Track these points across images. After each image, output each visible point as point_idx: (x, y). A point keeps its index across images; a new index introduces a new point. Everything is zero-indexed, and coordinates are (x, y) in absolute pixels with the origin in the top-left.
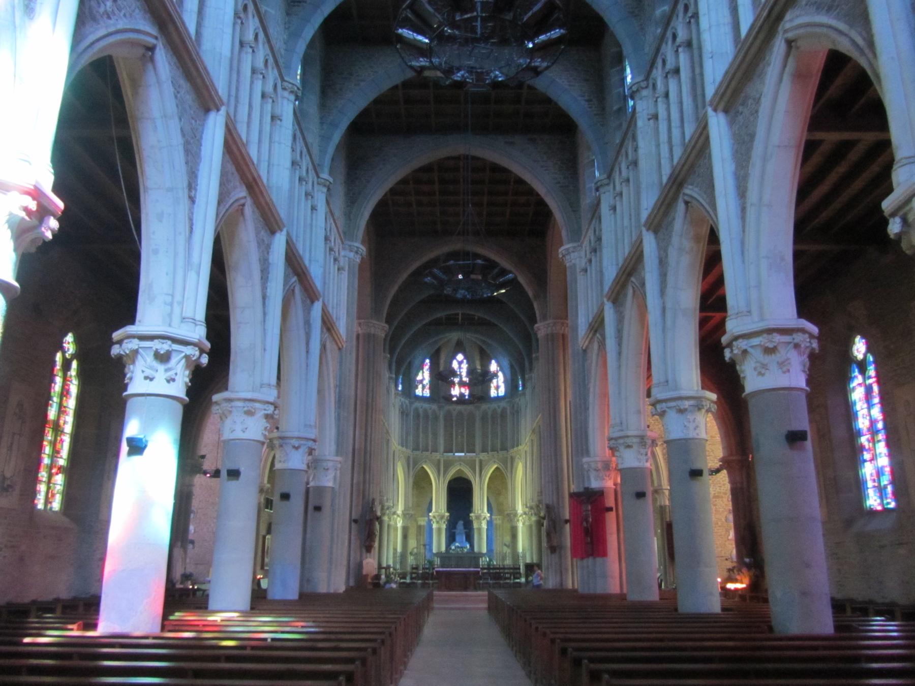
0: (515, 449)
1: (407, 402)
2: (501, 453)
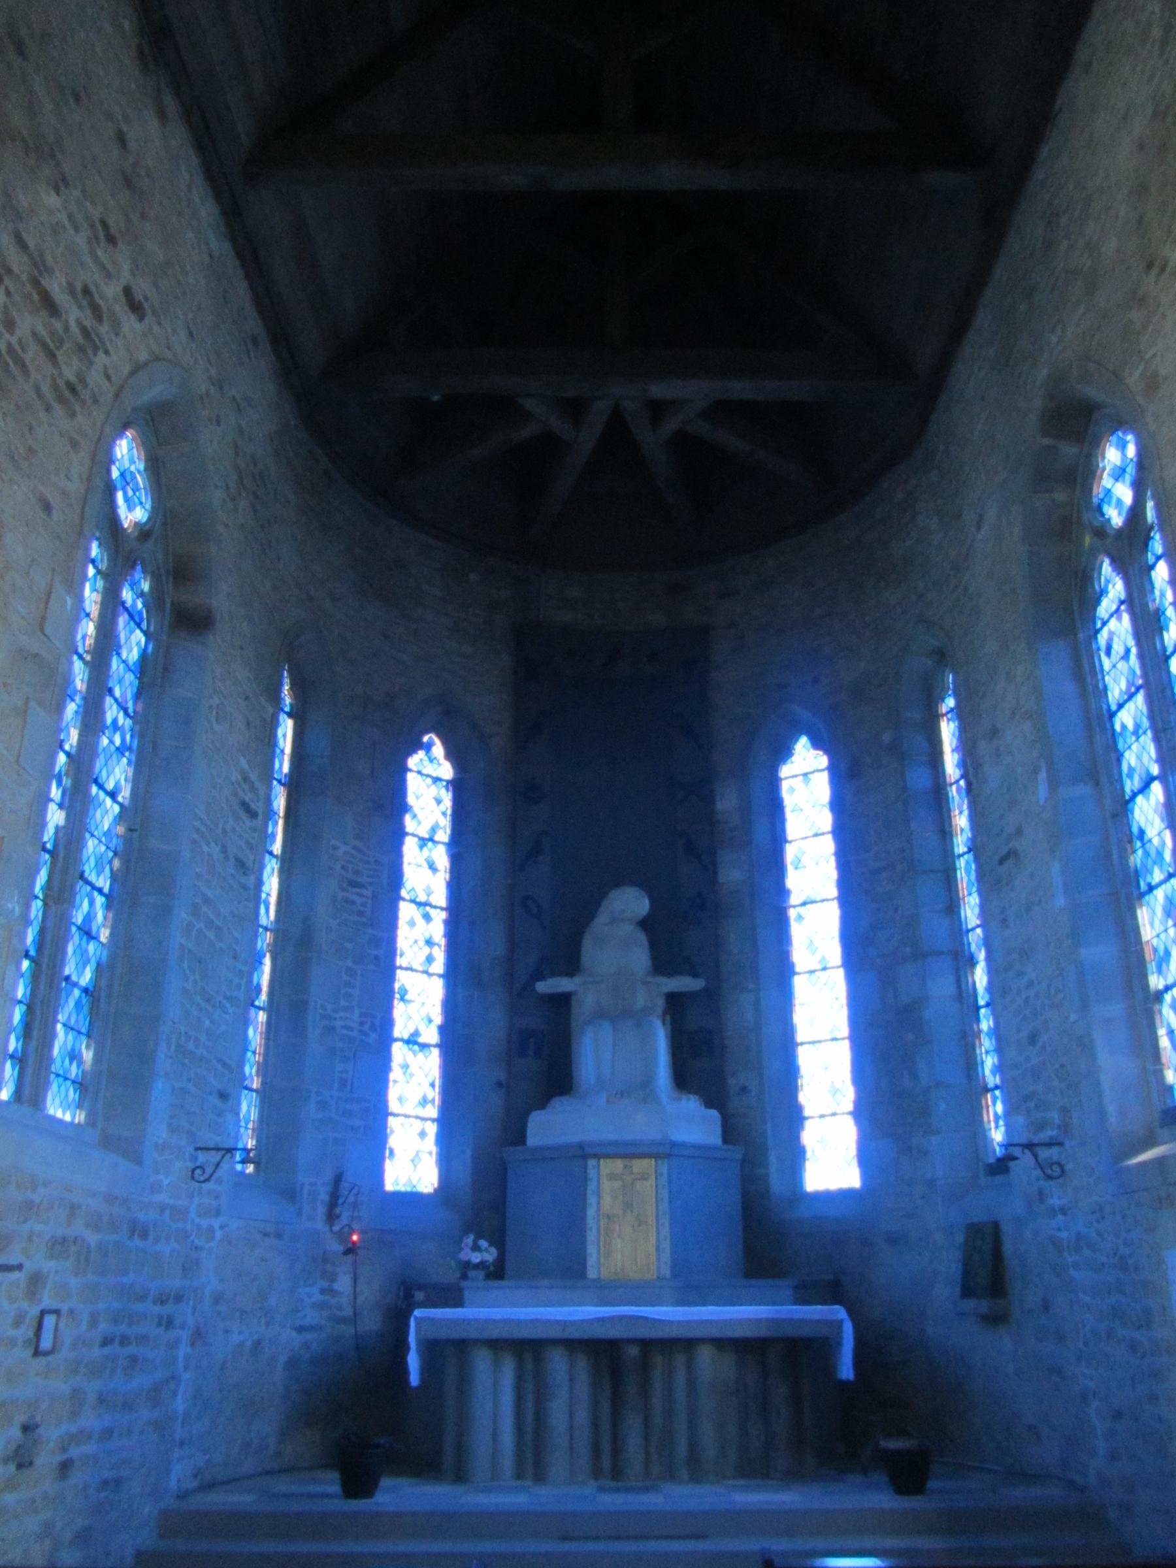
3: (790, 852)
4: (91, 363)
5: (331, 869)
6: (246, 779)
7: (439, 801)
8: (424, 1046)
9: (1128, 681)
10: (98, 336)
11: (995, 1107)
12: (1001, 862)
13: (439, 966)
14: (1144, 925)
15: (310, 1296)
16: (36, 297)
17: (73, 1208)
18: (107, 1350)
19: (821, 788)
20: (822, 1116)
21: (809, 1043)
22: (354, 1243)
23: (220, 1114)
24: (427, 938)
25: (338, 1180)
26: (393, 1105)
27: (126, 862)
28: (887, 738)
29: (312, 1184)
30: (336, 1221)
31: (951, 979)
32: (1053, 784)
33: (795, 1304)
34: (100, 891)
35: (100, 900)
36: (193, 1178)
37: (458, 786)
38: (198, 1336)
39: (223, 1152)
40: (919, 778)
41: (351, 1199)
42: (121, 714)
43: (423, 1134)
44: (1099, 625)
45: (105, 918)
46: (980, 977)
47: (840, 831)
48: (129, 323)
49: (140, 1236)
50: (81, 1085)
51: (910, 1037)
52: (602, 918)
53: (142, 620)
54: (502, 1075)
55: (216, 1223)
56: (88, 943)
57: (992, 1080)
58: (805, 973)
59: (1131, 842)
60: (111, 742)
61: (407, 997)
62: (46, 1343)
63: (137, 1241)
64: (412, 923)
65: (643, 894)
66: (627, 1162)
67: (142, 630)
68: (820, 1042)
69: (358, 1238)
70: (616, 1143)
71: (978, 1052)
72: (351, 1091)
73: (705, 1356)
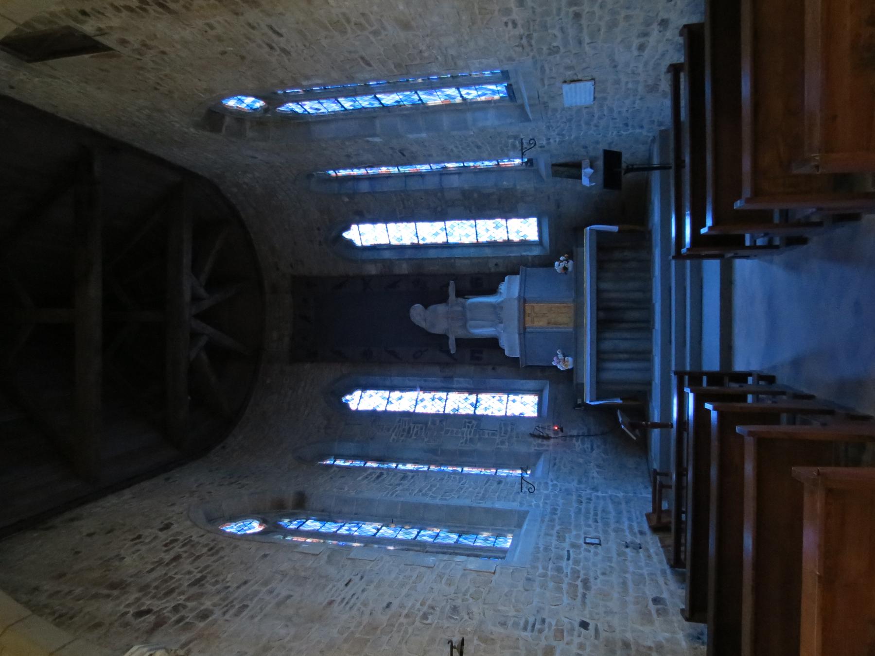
3: (394, 242)
4: (198, 543)
5: (402, 441)
6: (367, 477)
7: (371, 396)
8: (477, 401)
9: (332, 103)
10: (185, 540)
11: (506, 163)
12: (404, 155)
13: (443, 395)
14: (435, 103)
15: (579, 446)
16: (174, 564)
17: (547, 534)
18: (599, 521)
19: (366, 228)
20: (508, 232)
21: (477, 237)
22: (558, 428)
23: (507, 483)
24: (431, 400)
25: (533, 435)
26: (502, 413)
27: (406, 523)
28: (346, 200)
29: (535, 446)
30: (550, 435)
31: (452, 177)
32: (374, 135)
33: (584, 247)
34: (419, 533)
35: (422, 533)
36: (532, 492)
37: (364, 388)
38: (595, 489)
39: (523, 480)
40: (364, 187)
41: (541, 430)
42: (344, 528)
43: (514, 401)
44: (307, 113)
45: (429, 531)
46: (451, 165)
47: (386, 221)
48: (175, 528)
49: (556, 511)
50: (497, 536)
51: (476, 195)
52: (423, 325)
53: (301, 522)
54: (490, 367)
55: (550, 483)
56: (440, 536)
57: (494, 163)
58: (447, 238)
59: (400, 106)
60: (356, 531)
61: (457, 408)
62: (597, 541)
63: (558, 512)
64: (425, 407)
65: (413, 307)
66: (527, 315)
67: (306, 521)
68: (476, 232)
69: (557, 427)
70: (519, 321)
71: (482, 167)
72: (496, 431)
73: (604, 286)
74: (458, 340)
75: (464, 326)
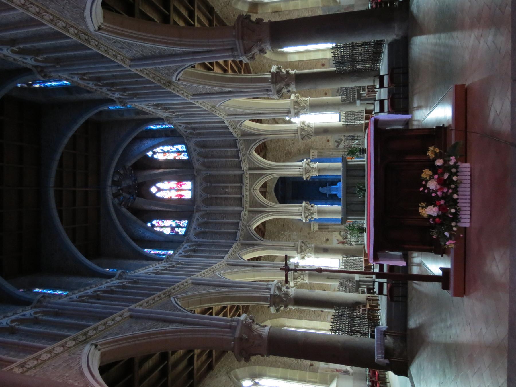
0: (231, 129)
1: (186, 245)
2: (239, 147)
74: (329, 195)
75: (330, 192)
